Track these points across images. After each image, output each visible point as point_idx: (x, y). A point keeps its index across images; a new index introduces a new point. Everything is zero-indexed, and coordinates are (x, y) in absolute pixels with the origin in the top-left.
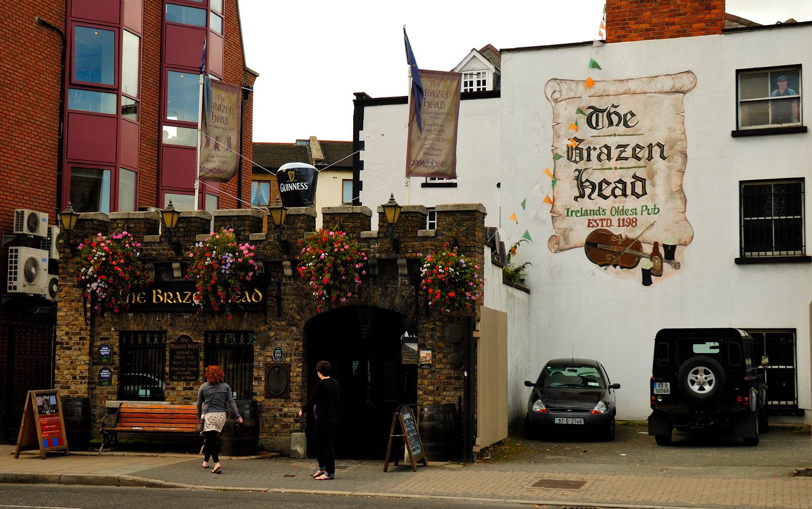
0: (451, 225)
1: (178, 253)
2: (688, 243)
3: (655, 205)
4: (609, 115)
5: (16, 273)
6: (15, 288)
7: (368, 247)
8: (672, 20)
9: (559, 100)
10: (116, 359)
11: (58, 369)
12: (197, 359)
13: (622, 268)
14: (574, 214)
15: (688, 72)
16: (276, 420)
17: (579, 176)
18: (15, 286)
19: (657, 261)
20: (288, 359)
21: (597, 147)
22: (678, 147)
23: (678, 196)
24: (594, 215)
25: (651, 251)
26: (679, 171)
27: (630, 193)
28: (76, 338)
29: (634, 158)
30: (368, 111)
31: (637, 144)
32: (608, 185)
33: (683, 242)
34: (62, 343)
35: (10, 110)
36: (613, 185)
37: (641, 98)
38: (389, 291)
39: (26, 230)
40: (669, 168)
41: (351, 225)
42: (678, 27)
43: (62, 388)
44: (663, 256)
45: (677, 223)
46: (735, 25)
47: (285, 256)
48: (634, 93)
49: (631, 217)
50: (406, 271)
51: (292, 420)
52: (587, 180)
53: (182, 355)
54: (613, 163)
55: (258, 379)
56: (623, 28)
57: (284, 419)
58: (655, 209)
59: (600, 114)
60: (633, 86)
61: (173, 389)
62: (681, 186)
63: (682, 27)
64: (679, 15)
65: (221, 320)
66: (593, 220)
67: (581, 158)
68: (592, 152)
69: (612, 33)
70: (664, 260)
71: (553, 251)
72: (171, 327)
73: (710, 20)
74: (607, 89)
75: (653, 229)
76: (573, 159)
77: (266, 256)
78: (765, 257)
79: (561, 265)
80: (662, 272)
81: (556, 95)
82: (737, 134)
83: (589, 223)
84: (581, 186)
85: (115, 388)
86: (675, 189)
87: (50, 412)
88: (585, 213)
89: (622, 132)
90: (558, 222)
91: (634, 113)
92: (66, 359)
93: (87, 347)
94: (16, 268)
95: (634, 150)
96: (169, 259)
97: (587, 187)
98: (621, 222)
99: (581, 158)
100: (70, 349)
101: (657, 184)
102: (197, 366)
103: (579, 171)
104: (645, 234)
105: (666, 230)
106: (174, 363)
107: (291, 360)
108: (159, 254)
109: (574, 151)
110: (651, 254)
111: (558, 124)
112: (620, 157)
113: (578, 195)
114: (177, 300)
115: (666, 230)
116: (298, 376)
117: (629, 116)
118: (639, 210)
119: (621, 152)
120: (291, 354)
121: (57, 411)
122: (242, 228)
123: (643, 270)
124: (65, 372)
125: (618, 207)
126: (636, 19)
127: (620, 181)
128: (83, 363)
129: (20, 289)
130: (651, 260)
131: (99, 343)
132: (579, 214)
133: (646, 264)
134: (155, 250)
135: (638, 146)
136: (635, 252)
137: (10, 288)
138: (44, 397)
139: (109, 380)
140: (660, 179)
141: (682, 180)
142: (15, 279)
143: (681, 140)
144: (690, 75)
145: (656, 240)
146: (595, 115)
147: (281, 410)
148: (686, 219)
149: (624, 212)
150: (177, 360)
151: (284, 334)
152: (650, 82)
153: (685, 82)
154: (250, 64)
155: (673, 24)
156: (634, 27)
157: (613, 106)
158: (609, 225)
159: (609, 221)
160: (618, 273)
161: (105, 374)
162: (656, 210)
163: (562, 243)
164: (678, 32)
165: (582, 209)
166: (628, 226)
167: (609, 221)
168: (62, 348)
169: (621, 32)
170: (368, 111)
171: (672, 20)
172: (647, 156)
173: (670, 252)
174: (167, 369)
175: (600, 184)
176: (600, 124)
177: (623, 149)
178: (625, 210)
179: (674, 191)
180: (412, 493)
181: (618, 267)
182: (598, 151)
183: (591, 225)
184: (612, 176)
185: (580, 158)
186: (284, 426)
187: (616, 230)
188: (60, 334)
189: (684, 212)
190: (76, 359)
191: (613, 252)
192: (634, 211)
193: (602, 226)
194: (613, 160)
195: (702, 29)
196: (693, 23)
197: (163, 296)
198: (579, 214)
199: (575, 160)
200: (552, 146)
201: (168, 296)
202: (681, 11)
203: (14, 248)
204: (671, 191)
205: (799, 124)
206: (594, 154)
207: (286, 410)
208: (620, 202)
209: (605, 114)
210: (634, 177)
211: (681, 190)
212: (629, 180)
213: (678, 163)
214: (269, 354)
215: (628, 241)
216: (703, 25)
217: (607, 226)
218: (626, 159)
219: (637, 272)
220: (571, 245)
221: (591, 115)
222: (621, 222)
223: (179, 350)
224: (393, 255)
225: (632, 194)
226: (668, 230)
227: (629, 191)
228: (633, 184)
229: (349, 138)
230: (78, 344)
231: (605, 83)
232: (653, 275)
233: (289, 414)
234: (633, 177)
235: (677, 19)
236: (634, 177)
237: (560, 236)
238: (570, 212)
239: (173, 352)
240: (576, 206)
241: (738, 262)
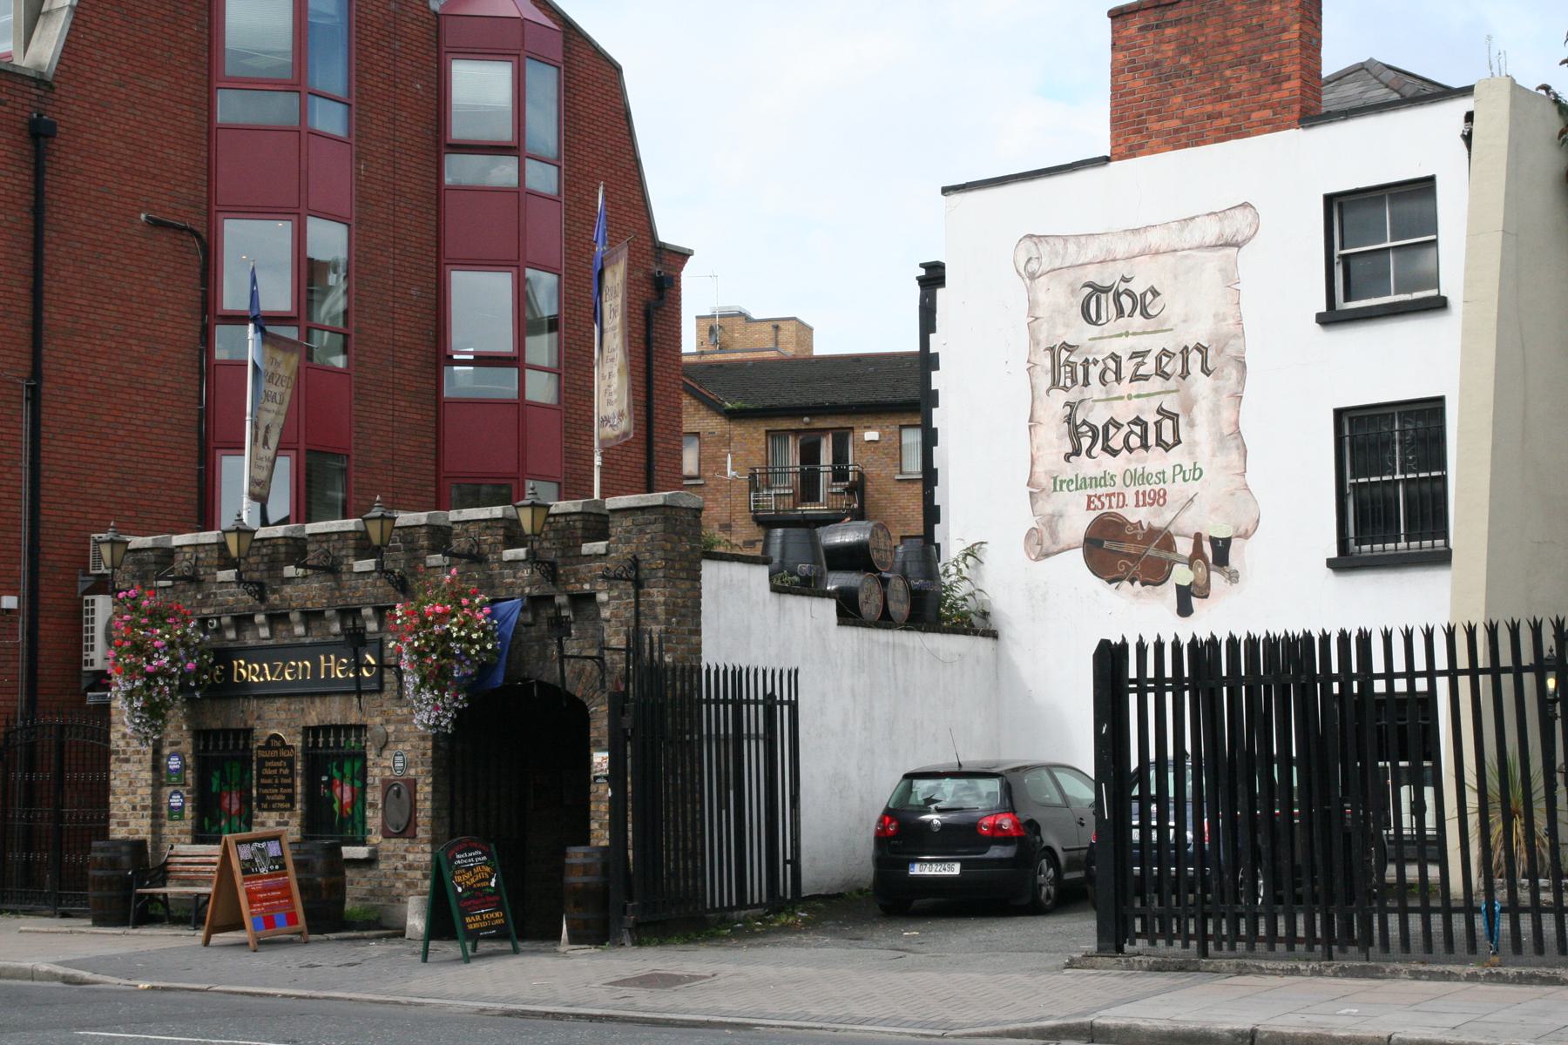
0: (629, 532)
1: (262, 599)
2: (1250, 532)
3: (1195, 464)
4: (1117, 295)
7: (515, 577)
8: (1219, 107)
9: (1037, 275)
10: (189, 775)
12: (292, 774)
13: (1143, 584)
14: (1064, 486)
15: (1245, 205)
16: (398, 874)
17: (1070, 414)
18: (92, 660)
19: (1200, 570)
20: (412, 772)
21: (1100, 358)
22: (1231, 351)
23: (1233, 444)
24: (1096, 486)
25: (1191, 551)
26: (1232, 396)
27: (1154, 443)
29: (1160, 376)
31: (1164, 349)
32: (1118, 429)
33: (1242, 530)
34: (118, 752)
35: (89, 372)
36: (1126, 429)
37: (1169, 260)
40: (1216, 390)
41: (490, 540)
42: (1227, 120)
44: (1211, 561)
45: (1232, 494)
46: (1430, 90)
48: (1157, 253)
49: (1157, 488)
52: (1084, 422)
53: (273, 768)
54: (1125, 387)
55: (373, 805)
56: (1139, 131)
58: (1195, 469)
59: (1103, 296)
60: (1155, 239)
62: (1237, 424)
63: (1232, 121)
64: (1229, 97)
65: (323, 707)
66: (1095, 496)
67: (1074, 382)
68: (1091, 367)
69: (1121, 140)
70: (1212, 566)
71: (1033, 557)
72: (258, 722)
73: (1279, 102)
74: (1112, 247)
75: (1194, 508)
76: (1062, 384)
77: (376, 598)
78: (1406, 551)
79: (1046, 583)
80: (1209, 588)
81: (1034, 266)
83: (1090, 502)
84: (1075, 434)
86: (1226, 431)
87: (269, 870)
88: (1083, 483)
89: (1139, 328)
90: (1040, 502)
91: (1158, 290)
92: (125, 778)
95: (1159, 360)
96: (250, 609)
97: (1084, 435)
98: (1141, 497)
99: (1074, 382)
100: (127, 761)
101: (1197, 422)
102: (292, 786)
104: (1179, 520)
105: (1214, 510)
106: (263, 781)
107: (417, 772)
108: (238, 601)
109: (1062, 369)
110: (1191, 556)
111: (1037, 319)
112: (1136, 376)
113: (1070, 450)
114: (265, 676)
115: (1214, 510)
116: (426, 799)
117: (1149, 297)
118: (1169, 474)
119: (1139, 365)
120: (416, 763)
121: (283, 867)
122: (344, 553)
123: (1179, 588)
124: (123, 799)
125: (1136, 470)
126: (1159, 111)
127: (1138, 421)
128: (144, 784)
130: (1191, 568)
132: (1073, 487)
133: (1182, 575)
134: (232, 595)
135: (1165, 352)
136: (1164, 554)
138: (255, 844)
139: (181, 808)
140: (1201, 413)
141: (1239, 412)
143: (1235, 336)
144: (1248, 210)
145: (1197, 530)
146: (1094, 298)
147: (404, 858)
148: (1246, 488)
149: (1144, 478)
150: (267, 777)
152: (1182, 230)
153: (1239, 224)
154: (667, 233)
155: (1220, 115)
156: (1156, 126)
157: (1125, 280)
158: (1121, 504)
159: (1121, 497)
160: (1137, 595)
162: (1197, 474)
163: (1047, 542)
164: (1227, 130)
165: (1077, 476)
166: (1151, 505)
167: (1121, 497)
168: (118, 760)
171: (1219, 107)
172: (1179, 370)
173: (1222, 550)
174: (254, 792)
175: (1106, 428)
176: (1103, 314)
177: (1141, 359)
178: (1145, 475)
179: (1226, 433)
181: (1137, 583)
182: (1100, 366)
183: (1092, 506)
184: (1124, 413)
185: (1073, 381)
187: (1135, 515)
189: (1243, 474)
190: (136, 778)
191: (1128, 556)
192: (1161, 476)
193: (1110, 507)
195: (1266, 122)
196: (1252, 111)
197: (246, 669)
198: (1073, 487)
199: (1065, 386)
200: (1029, 361)
202: (1232, 91)
204: (1221, 434)
205: (1432, 293)
206: (1095, 372)
207: (410, 857)
208: (1137, 461)
209: (1111, 294)
210: (1160, 411)
211: (1237, 433)
212: (1151, 418)
213: (1231, 382)
214: (387, 763)
215: (1152, 533)
216: (1268, 113)
217: (1118, 507)
218: (1146, 378)
219: (1169, 593)
220: (1061, 546)
222: (1141, 497)
223: (269, 759)
225: (1157, 445)
226: (1217, 509)
227: (1152, 439)
228: (1158, 424)
229: (915, 347)
231: (1110, 237)
232: (1195, 596)
233: (416, 864)
234: (1158, 412)
235: (1225, 107)
237: (1042, 527)
238: (1058, 483)
240: (1068, 471)
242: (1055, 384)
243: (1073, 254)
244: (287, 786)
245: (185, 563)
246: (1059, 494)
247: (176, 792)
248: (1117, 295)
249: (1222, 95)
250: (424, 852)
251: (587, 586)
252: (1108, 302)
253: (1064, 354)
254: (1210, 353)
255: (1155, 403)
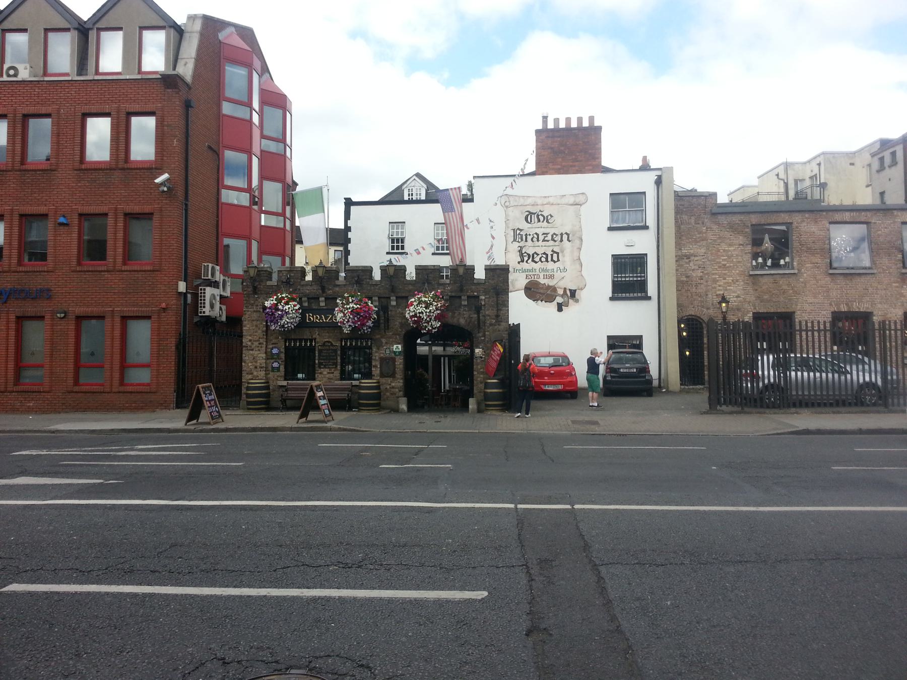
1: (323, 289)
4: (538, 216)
5: (204, 303)
6: (204, 312)
8: (574, 164)
10: (283, 356)
11: (245, 362)
12: (336, 355)
28: (256, 344)
30: (353, 209)
33: (580, 287)
36: (540, 256)
37: (557, 207)
38: (456, 315)
39: (210, 277)
43: (247, 374)
47: (393, 294)
48: (552, 204)
50: (466, 303)
51: (397, 390)
52: (525, 252)
54: (540, 243)
55: (376, 366)
57: (392, 390)
59: (533, 215)
60: (551, 200)
61: (321, 373)
64: (577, 161)
67: (522, 240)
68: (528, 236)
81: (507, 204)
82: (610, 229)
84: (522, 255)
85: (283, 374)
88: (524, 271)
93: (264, 348)
94: (204, 300)
95: (552, 236)
97: (525, 256)
99: (522, 240)
100: (252, 350)
103: (521, 247)
104: (558, 284)
114: (323, 320)
116: (400, 364)
117: (549, 217)
118: (555, 270)
119: (545, 237)
122: (364, 277)
124: (250, 364)
127: (544, 253)
129: (207, 314)
131: (271, 347)
133: (559, 300)
135: (554, 234)
137: (201, 313)
140: (567, 252)
142: (204, 307)
147: (390, 384)
149: (547, 270)
151: (391, 340)
153: (581, 199)
155: (575, 166)
157: (540, 211)
161: (276, 365)
162: (565, 270)
169: (545, 170)
170: (353, 209)
171: (574, 164)
173: (573, 293)
174: (317, 361)
180: (515, 430)
182: (532, 236)
184: (540, 251)
186: (391, 394)
187: (542, 281)
188: (245, 341)
189: (581, 271)
191: (540, 293)
194: (540, 242)
201: (317, 318)
203: (203, 288)
206: (529, 238)
207: (393, 384)
208: (544, 265)
210: (553, 251)
212: (549, 253)
215: (549, 287)
218: (548, 241)
221: (528, 215)
224: (459, 294)
227: (549, 259)
230: (258, 347)
235: (576, 163)
236: (553, 251)
239: (320, 351)
240: (519, 267)
241: (612, 299)
242: (515, 240)
243: (522, 201)
244: (334, 359)
245: (283, 277)
246: (515, 274)
247: (276, 362)
248: (538, 216)
249: (576, 160)
250: (399, 382)
251: (476, 294)
252: (534, 218)
253: (518, 232)
254: (570, 236)
255: (551, 249)
